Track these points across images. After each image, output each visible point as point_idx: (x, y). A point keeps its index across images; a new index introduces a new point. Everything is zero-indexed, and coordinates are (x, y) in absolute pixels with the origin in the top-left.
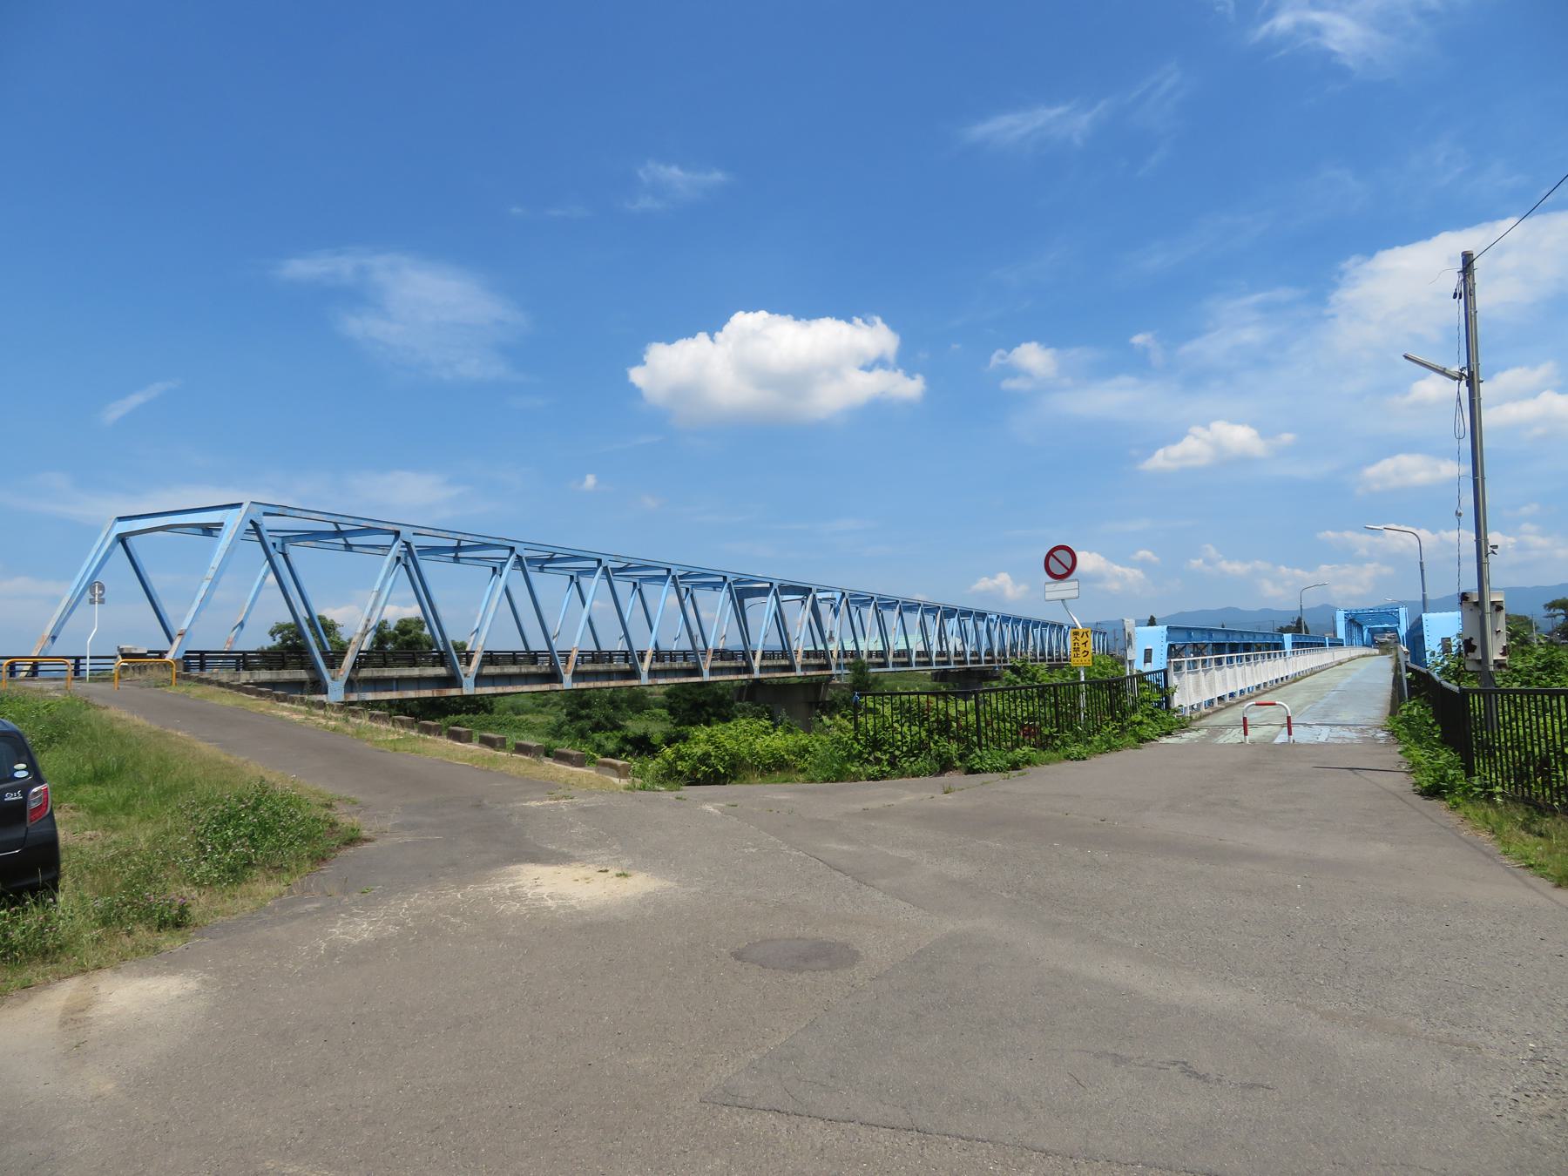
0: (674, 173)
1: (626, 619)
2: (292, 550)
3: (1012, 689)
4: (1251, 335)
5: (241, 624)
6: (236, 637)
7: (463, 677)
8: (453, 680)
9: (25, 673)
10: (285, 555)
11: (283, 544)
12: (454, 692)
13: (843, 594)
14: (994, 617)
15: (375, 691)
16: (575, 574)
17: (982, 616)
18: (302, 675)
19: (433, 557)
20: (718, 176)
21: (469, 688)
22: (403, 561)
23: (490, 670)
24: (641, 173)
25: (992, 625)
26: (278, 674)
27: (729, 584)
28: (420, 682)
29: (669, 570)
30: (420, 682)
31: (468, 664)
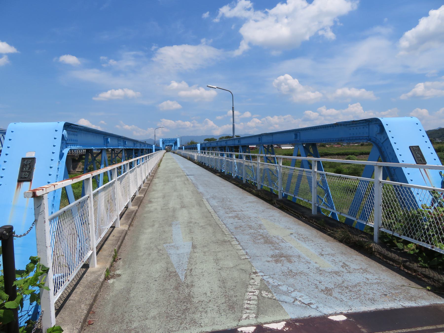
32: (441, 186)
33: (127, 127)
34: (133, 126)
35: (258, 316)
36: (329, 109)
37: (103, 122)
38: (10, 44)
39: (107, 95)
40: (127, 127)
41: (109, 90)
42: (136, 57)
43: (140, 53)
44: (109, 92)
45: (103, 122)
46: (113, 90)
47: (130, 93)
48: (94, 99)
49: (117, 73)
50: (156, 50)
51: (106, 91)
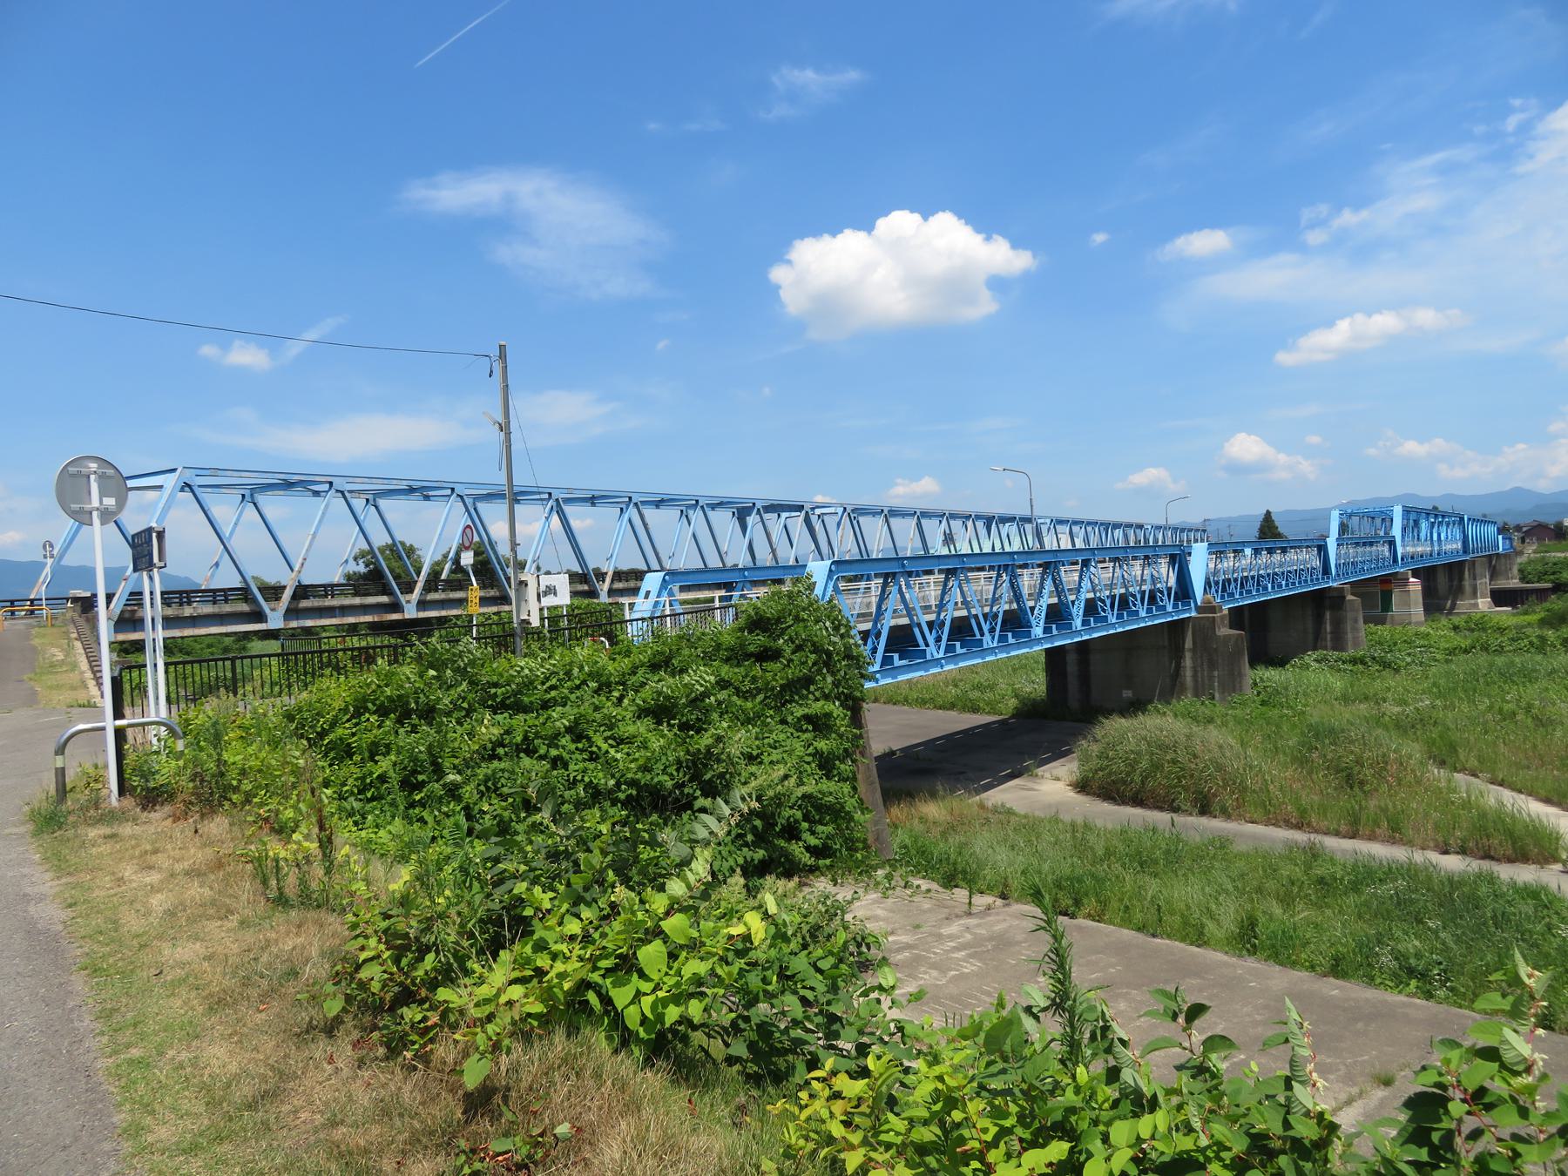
0: (808, 77)
1: (774, 539)
2: (480, 506)
3: (482, 638)
4: (1425, 201)
5: (217, 564)
6: (212, 575)
7: (404, 603)
8: (396, 607)
9: (23, 613)
10: (475, 509)
11: (252, 495)
12: (395, 617)
13: (845, 509)
14: (1150, 527)
15: (297, 619)
16: (684, 508)
17: (1140, 527)
18: (384, 599)
19: (282, 493)
20: (853, 75)
21: (411, 612)
22: (371, 502)
23: (632, 584)
24: (775, 79)
25: (1147, 535)
26: (220, 608)
27: (702, 507)
28: (365, 609)
29: (453, 489)
30: (365, 609)
31: (604, 581)
32: (1438, 495)
33: (1411, 447)
34: (1439, 441)
35: (234, 920)
36: (988, 239)
37: (1315, 439)
38: (984, 221)
39: (1339, 335)
40: (1411, 447)
41: (1342, 318)
42: (1447, 170)
43: (1463, 153)
44: (1343, 325)
45: (1315, 439)
46: (1359, 317)
47: (1426, 317)
48: (1284, 358)
49: (1363, 251)
50: (1525, 129)
51: (1330, 324)
